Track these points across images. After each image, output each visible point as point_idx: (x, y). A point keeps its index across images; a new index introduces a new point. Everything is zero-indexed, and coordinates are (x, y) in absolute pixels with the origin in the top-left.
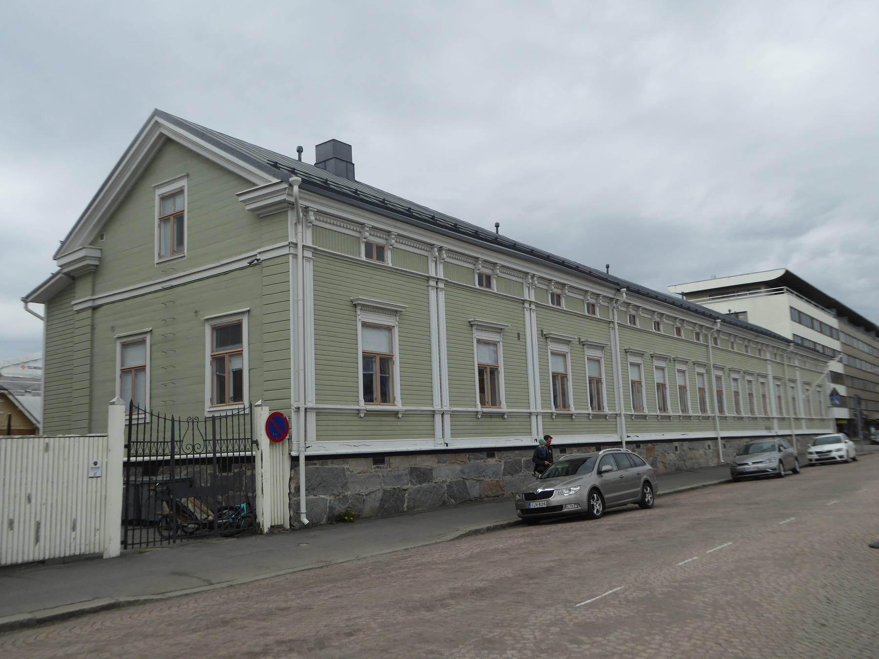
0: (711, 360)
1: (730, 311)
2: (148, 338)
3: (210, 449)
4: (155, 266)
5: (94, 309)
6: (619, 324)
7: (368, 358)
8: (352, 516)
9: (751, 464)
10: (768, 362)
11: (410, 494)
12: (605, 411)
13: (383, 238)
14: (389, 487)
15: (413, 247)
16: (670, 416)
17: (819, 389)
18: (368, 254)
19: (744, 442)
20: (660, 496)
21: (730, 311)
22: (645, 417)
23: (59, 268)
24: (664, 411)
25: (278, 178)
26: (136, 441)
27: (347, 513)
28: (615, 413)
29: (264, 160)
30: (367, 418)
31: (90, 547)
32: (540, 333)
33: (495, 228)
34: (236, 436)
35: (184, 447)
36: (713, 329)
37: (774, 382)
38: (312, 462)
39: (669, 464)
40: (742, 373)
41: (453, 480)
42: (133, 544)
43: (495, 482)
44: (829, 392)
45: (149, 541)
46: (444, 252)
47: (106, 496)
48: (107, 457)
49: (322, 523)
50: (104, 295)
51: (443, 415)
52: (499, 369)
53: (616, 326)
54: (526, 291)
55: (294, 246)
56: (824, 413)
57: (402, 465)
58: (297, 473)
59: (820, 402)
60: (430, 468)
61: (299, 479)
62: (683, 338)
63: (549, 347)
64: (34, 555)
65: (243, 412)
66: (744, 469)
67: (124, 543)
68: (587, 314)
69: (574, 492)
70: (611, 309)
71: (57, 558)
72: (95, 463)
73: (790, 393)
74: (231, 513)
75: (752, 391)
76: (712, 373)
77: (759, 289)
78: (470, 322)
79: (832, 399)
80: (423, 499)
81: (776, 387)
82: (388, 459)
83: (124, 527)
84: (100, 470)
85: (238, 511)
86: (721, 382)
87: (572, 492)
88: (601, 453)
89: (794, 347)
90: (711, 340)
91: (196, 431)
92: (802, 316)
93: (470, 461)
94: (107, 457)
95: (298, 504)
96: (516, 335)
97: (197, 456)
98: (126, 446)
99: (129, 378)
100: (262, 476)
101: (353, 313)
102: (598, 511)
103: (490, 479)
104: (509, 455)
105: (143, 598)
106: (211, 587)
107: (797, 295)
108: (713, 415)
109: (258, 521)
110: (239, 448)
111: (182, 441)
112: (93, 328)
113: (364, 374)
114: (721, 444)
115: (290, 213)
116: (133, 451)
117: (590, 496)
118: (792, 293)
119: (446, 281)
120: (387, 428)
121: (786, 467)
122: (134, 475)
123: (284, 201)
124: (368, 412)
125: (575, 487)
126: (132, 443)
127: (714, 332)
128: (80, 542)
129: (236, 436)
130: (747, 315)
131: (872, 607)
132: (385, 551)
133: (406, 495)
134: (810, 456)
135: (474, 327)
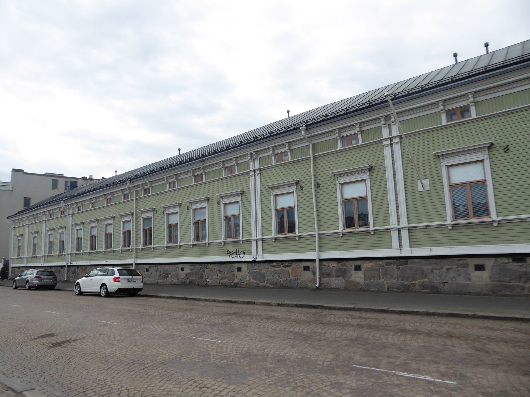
29: (212, 152)
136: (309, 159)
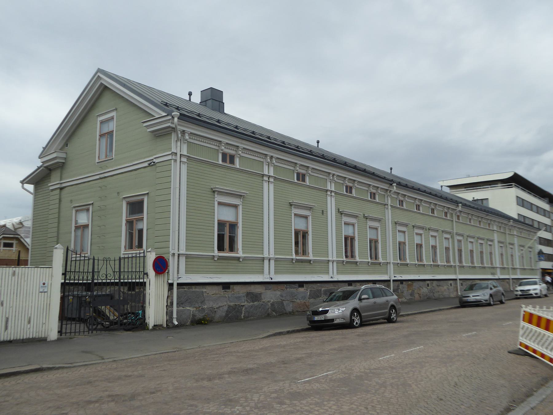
0: (455, 229)
1: (474, 198)
2: (91, 207)
3: (117, 277)
4: (96, 164)
5: (61, 189)
6: (392, 206)
7: (221, 224)
8: (207, 321)
9: (472, 296)
10: (495, 232)
11: (246, 308)
12: (379, 260)
13: (234, 150)
14: (232, 304)
15: (254, 156)
16: (425, 265)
17: (530, 250)
18: (224, 160)
19: (469, 283)
20: (402, 316)
21: (474, 198)
22: (407, 265)
23: (42, 164)
24: (421, 261)
25: (166, 112)
26: (70, 271)
27: (204, 319)
28: (387, 262)
29: (158, 100)
30: (219, 261)
31: (39, 334)
32: (337, 210)
33: (390, 170)
34: (134, 270)
35: (100, 275)
36: (456, 210)
37: (498, 245)
38: (182, 287)
39: (423, 294)
40: (476, 238)
41: (275, 301)
42: (66, 333)
43: (303, 303)
44: (537, 251)
45: (76, 331)
46: (274, 159)
47: (50, 304)
48: (51, 281)
49: (187, 324)
50: (67, 181)
51: (269, 260)
52: (309, 233)
53: (390, 207)
54: (329, 184)
55: (175, 154)
56: (533, 265)
57: (242, 291)
58: (172, 293)
59: (531, 258)
60: (260, 293)
61: (173, 297)
62: (436, 216)
63: (343, 219)
64: (33, 335)
65: (139, 255)
66: (467, 299)
67: (60, 332)
68: (370, 199)
69: (342, 311)
70: (386, 196)
71: (31, 338)
72: (44, 284)
73: (509, 251)
74: (133, 316)
75: (483, 250)
76: (455, 238)
77: (497, 184)
78: (290, 203)
79: (539, 257)
80: (254, 312)
81: (500, 248)
82: (232, 287)
83: (60, 321)
84: (47, 288)
85: (137, 315)
86: (461, 243)
87: (340, 311)
88: (363, 287)
89: (513, 222)
90: (455, 217)
91: (108, 266)
92: (525, 202)
93: (287, 289)
94: (51, 281)
95: (172, 312)
96: (321, 212)
97: (108, 281)
98: (63, 274)
99: (79, 232)
100: (149, 294)
101: (213, 196)
102: (357, 323)
103: (300, 301)
104: (314, 286)
105: (57, 366)
106: (103, 361)
107: (522, 189)
108: (454, 264)
109: (146, 322)
110: (136, 277)
111: (99, 272)
112: (60, 200)
113: (218, 234)
114: (459, 282)
115: (173, 134)
116: (68, 277)
117: (352, 314)
118: (518, 187)
119: (275, 177)
120: (233, 267)
121: (494, 299)
122: (77, 290)
123: (169, 127)
124: (220, 258)
125: (343, 308)
126: (67, 273)
127: (457, 212)
128: (33, 331)
129: (130, 270)
130: (488, 200)
131: (481, 389)
132: (217, 343)
133: (244, 309)
134: (516, 293)
135: (293, 206)
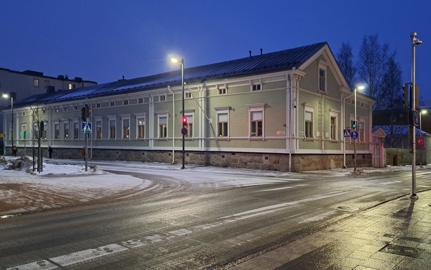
136: (170, 102)
